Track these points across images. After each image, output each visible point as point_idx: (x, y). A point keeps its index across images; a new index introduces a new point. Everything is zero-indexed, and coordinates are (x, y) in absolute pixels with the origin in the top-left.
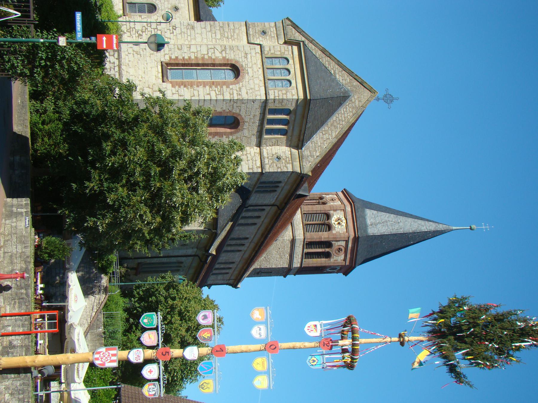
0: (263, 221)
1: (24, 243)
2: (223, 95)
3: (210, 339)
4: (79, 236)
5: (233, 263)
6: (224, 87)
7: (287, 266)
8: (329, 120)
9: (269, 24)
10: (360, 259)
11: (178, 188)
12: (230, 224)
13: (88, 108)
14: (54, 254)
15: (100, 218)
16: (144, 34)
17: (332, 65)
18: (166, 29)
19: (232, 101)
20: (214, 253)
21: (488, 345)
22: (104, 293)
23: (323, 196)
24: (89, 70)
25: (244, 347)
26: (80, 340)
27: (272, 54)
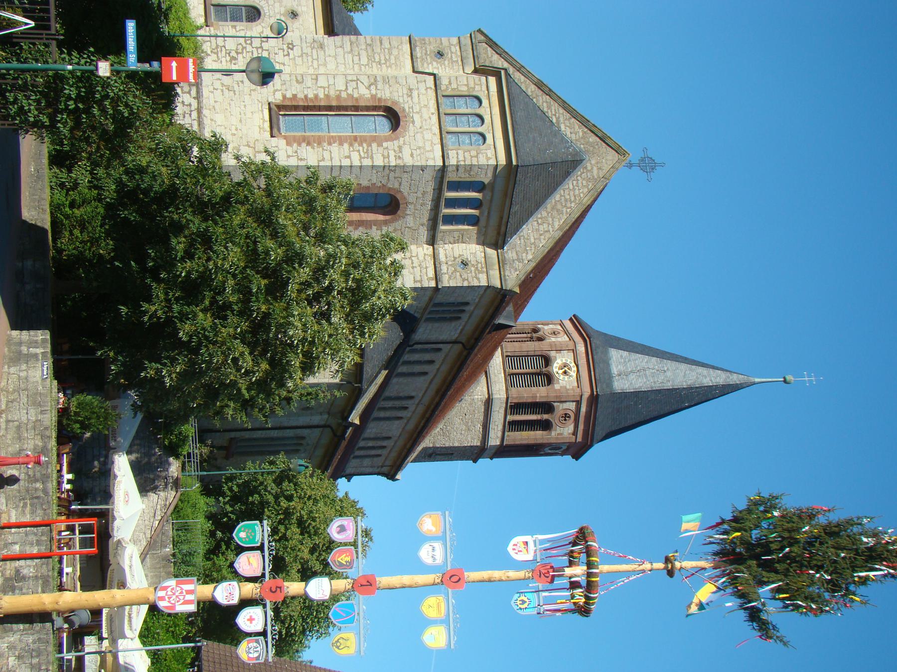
0: (438, 369)
1: (41, 406)
2: (372, 158)
3: (350, 565)
4: (132, 393)
5: (389, 438)
6: (374, 145)
7: (479, 444)
8: (549, 201)
9: (449, 40)
10: (599, 432)
11: (297, 313)
12: (384, 373)
13: (147, 180)
14: (90, 424)
15: (166, 363)
16: (240, 56)
17: (553, 108)
18: (276, 49)
19: (387, 169)
20: (357, 422)
21: (813, 576)
22: (174, 488)
23: (539, 326)
24: (148, 117)
25: (407, 579)
26: (134, 567)
27: (453, 89)
